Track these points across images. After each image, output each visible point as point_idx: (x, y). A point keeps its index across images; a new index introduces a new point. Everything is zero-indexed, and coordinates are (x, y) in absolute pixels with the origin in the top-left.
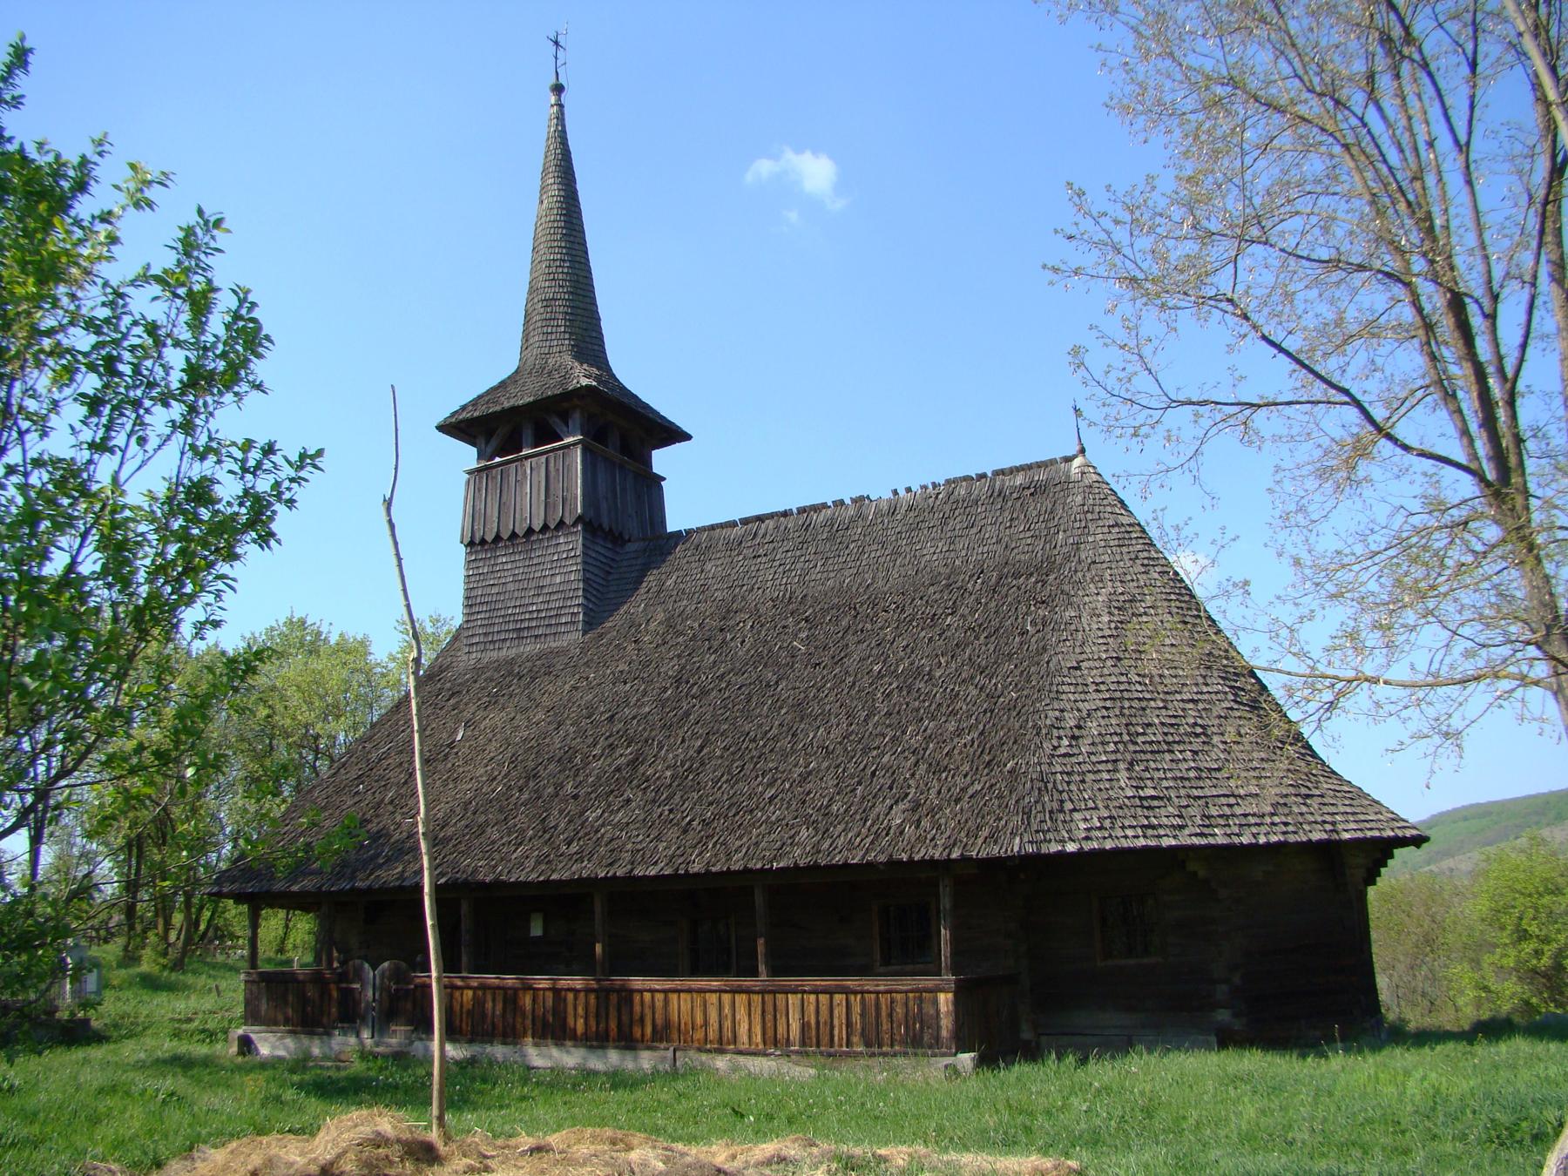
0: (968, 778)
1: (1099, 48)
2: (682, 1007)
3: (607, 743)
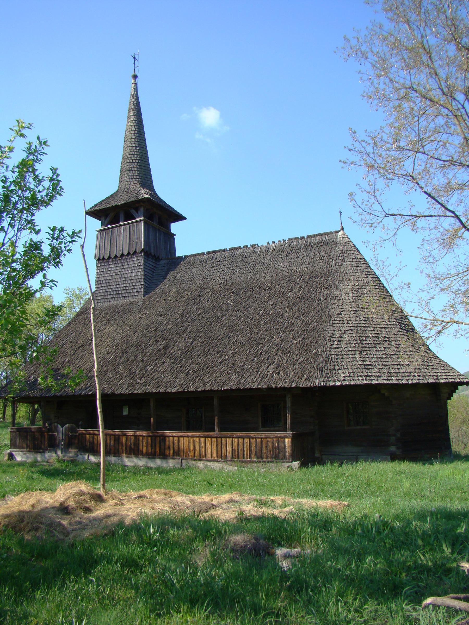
0: (298, 356)
1: (360, 72)
2: (185, 443)
3: (154, 339)
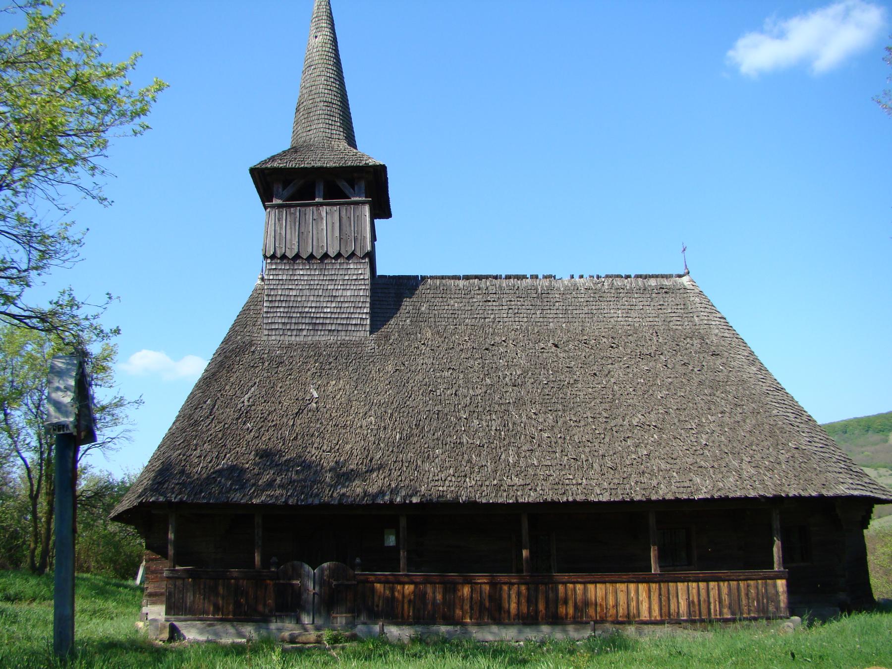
2: (597, 592)
